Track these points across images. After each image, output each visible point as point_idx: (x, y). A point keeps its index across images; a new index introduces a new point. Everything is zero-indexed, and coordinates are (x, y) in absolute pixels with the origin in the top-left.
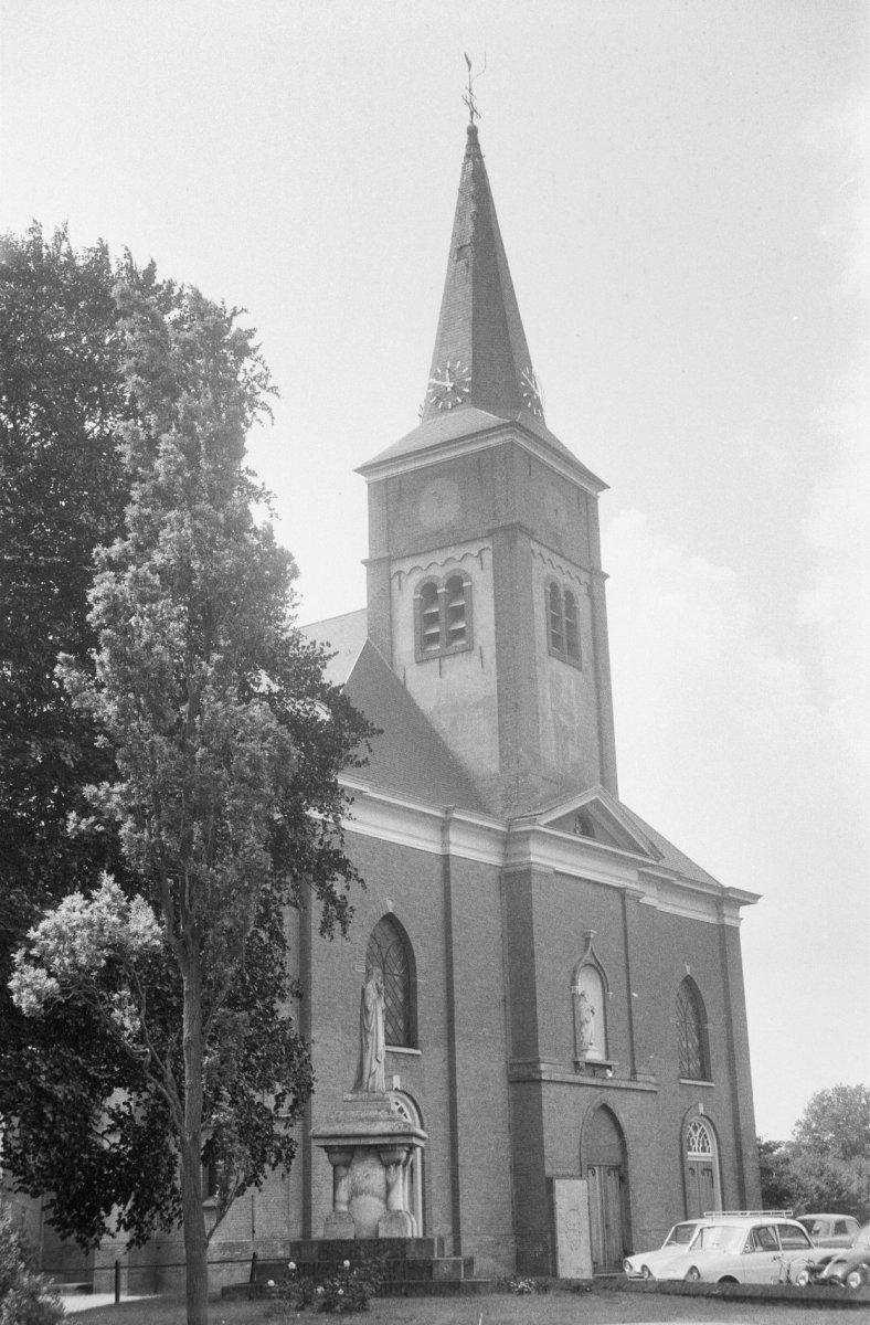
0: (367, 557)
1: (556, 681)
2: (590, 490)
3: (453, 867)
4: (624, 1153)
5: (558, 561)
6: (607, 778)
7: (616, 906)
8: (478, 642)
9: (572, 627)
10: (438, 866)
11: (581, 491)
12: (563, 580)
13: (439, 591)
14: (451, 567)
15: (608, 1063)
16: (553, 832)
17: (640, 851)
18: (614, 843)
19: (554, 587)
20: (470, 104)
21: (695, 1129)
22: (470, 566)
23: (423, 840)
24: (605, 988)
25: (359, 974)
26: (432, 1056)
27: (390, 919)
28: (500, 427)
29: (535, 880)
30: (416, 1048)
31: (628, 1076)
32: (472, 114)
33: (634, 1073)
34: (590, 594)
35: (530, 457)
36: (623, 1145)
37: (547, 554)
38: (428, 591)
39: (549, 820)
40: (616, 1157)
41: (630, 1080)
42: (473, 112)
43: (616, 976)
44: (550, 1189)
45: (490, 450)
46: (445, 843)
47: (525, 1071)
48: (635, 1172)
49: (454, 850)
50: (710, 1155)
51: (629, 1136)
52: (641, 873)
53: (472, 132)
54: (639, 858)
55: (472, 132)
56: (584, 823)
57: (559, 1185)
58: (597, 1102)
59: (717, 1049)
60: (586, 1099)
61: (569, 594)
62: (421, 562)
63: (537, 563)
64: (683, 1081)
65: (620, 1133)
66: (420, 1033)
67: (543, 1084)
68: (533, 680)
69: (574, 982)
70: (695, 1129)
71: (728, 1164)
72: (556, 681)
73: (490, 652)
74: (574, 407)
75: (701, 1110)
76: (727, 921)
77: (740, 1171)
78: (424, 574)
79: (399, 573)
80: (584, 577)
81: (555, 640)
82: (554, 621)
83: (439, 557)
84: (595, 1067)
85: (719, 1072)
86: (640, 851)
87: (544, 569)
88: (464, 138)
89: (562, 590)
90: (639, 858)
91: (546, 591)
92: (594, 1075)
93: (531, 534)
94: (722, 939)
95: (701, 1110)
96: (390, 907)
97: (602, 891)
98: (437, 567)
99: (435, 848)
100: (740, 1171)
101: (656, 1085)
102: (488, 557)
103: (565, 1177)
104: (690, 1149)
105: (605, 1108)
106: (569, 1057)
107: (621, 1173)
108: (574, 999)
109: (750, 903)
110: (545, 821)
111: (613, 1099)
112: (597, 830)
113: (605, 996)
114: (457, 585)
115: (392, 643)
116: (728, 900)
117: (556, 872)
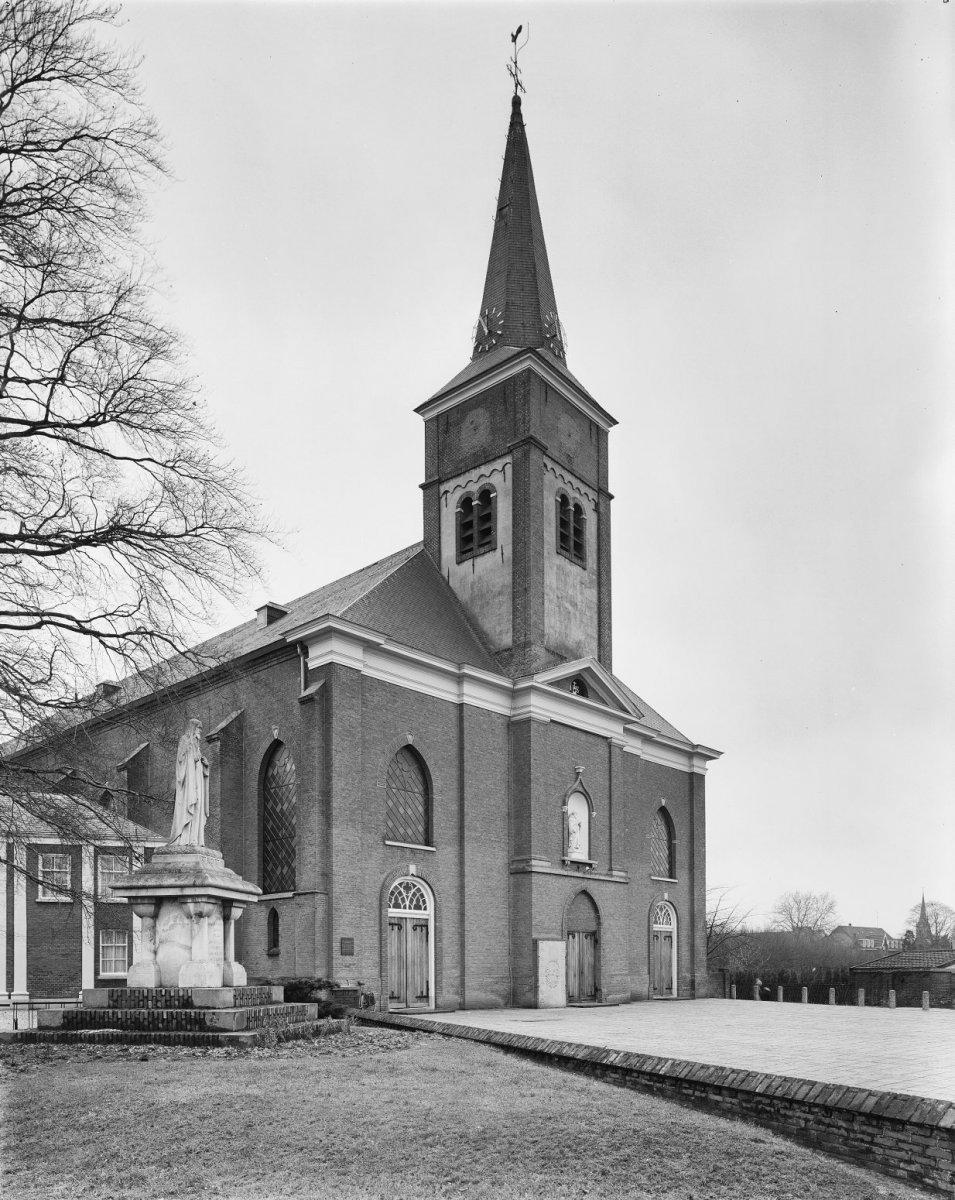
0: (423, 481)
1: (558, 575)
2: (602, 424)
3: (466, 712)
4: (599, 924)
5: (568, 477)
6: (604, 656)
7: (603, 750)
8: (500, 542)
9: (579, 532)
10: (453, 714)
11: (595, 426)
12: (572, 494)
13: (473, 504)
14: (484, 481)
15: (591, 862)
16: (550, 689)
17: (625, 711)
18: (604, 702)
19: (564, 499)
20: (515, 76)
21: (661, 910)
22: (496, 480)
23: (441, 689)
24: (591, 809)
25: (380, 789)
26: (445, 853)
27: (409, 749)
28: (518, 355)
29: (534, 726)
30: (675, 878)
31: (605, 872)
32: (516, 86)
33: (611, 869)
34: (597, 510)
35: (547, 386)
36: (598, 918)
37: (559, 470)
38: (466, 502)
39: (547, 678)
40: (592, 927)
41: (607, 875)
42: (518, 84)
43: (601, 802)
44: (535, 943)
45: (513, 379)
46: (461, 695)
47: (521, 866)
48: (606, 937)
49: (466, 700)
50: (673, 927)
51: (602, 912)
52: (625, 730)
53: (516, 102)
54: (622, 714)
55: (516, 102)
56: (581, 684)
57: (542, 945)
58: (579, 888)
59: (682, 857)
60: (569, 887)
61: (578, 507)
62: (461, 480)
63: (548, 477)
64: (388, 842)
65: (596, 910)
66: (435, 836)
67: (535, 878)
68: (541, 572)
69: (564, 803)
70: (661, 910)
71: (685, 933)
72: (558, 575)
73: (508, 551)
74: (592, 356)
75: (666, 896)
76: (696, 770)
77: (692, 937)
78: (464, 491)
79: (446, 492)
80: (592, 495)
81: (563, 538)
82: (563, 523)
83: (474, 474)
84: (578, 865)
85: (682, 875)
86: (625, 711)
87: (551, 485)
88: (509, 110)
89: (571, 502)
90: (622, 714)
91: (556, 500)
92: (578, 869)
93: (544, 450)
94: (691, 784)
95: (666, 896)
96: (410, 739)
97: (591, 739)
98: (471, 482)
99: (454, 699)
100: (692, 937)
101: (625, 878)
102: (509, 470)
103: (544, 940)
104: (656, 922)
105: (585, 892)
106: (558, 857)
107: (595, 937)
108: (564, 817)
109: (715, 758)
110: (543, 680)
111: (594, 889)
112: (590, 693)
113: (590, 815)
114: (486, 495)
115: (440, 551)
116: (696, 753)
117: (552, 721)
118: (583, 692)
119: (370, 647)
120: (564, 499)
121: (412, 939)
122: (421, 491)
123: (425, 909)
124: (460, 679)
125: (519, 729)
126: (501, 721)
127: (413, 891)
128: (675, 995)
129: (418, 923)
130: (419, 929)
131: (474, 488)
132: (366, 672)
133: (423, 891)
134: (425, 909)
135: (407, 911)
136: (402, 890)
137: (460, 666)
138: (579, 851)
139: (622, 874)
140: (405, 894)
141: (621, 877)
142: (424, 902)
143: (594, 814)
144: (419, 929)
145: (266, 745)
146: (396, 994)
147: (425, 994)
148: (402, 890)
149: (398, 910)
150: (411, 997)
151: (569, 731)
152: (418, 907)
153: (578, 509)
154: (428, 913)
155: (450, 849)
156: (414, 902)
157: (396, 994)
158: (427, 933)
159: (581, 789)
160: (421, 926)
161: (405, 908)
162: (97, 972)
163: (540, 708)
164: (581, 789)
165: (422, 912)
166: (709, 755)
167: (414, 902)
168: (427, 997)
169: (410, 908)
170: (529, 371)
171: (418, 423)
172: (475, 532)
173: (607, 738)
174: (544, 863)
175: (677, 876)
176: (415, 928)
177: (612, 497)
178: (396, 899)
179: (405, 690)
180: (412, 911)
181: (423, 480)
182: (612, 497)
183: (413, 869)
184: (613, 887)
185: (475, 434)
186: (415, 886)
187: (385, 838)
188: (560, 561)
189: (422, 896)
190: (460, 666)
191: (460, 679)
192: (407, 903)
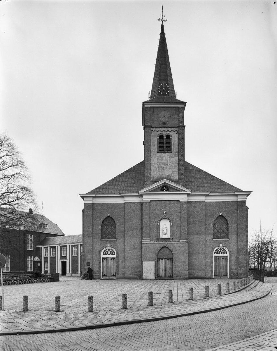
7: (177, 204)
24: (170, 223)
64: (214, 239)
96: (221, 214)
99: (236, 200)
109: (250, 194)
111: (169, 245)
113: (170, 224)
117: (151, 201)
118: (167, 190)
119: (206, 196)
121: (110, 262)
123: (227, 254)
126: (139, 204)
128: (228, 278)
130: (113, 259)
132: (94, 202)
133: (226, 249)
134: (115, 254)
135: (109, 255)
137: (234, 192)
139: (186, 240)
141: (186, 241)
142: (226, 252)
143: (172, 224)
144: (113, 259)
146: (105, 275)
147: (114, 275)
149: (106, 255)
150: (110, 275)
152: (112, 254)
154: (115, 256)
155: (121, 239)
156: (111, 253)
158: (227, 260)
159: (166, 218)
160: (113, 259)
161: (220, 254)
162: (44, 269)
166: (247, 194)
168: (115, 276)
169: (110, 255)
173: (179, 200)
174: (149, 240)
175: (229, 237)
176: (111, 259)
177: (185, 126)
178: (106, 253)
179: (107, 204)
180: (104, 255)
183: (108, 245)
184: (180, 245)
186: (223, 248)
187: (100, 239)
189: (226, 251)
190: (234, 192)
191: (141, 196)
192: (109, 253)
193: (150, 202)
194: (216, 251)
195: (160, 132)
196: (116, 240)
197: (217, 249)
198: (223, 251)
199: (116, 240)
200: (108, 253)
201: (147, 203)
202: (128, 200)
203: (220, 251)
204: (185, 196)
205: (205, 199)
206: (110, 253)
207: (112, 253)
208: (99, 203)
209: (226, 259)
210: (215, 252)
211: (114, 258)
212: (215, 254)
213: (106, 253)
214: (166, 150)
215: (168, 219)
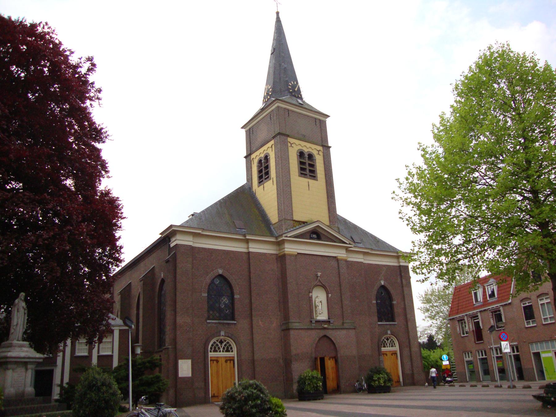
7: (334, 263)
14: (265, 152)
21: (388, 339)
24: (327, 294)
38: (260, 162)
60: (315, 335)
64: (208, 321)
74: (312, 94)
83: (261, 150)
96: (221, 272)
99: (245, 250)
111: (329, 333)
114: (266, 158)
117: (298, 253)
118: (319, 238)
119: (365, 253)
120: (301, 154)
122: (245, 159)
123: (232, 351)
124: (247, 241)
125: (282, 258)
127: (224, 343)
129: (228, 358)
130: (229, 362)
131: (262, 156)
132: (349, 259)
133: (230, 343)
134: (232, 351)
135: (221, 353)
136: (218, 343)
138: (322, 315)
140: (220, 345)
142: (231, 348)
144: (229, 362)
145: (159, 281)
148: (218, 343)
149: (216, 353)
151: (313, 257)
152: (227, 351)
153: (311, 156)
157: (216, 395)
159: (320, 284)
160: (230, 360)
161: (220, 351)
163: (290, 249)
164: (320, 284)
165: (231, 353)
167: (213, 349)
169: (223, 351)
170: (278, 107)
171: (244, 131)
172: (264, 173)
176: (392, 355)
177: (330, 147)
178: (215, 348)
181: (245, 155)
182: (330, 147)
185: (263, 134)
188: (304, 181)
189: (230, 345)
190: (245, 236)
191: (247, 241)
192: (222, 350)
193: (296, 255)
194: (212, 345)
195: (300, 147)
196: (235, 322)
197: (214, 343)
198: (225, 345)
199: (235, 322)
200: (219, 348)
201: (291, 255)
202: (255, 248)
203: (220, 345)
204: (344, 251)
205: (194, 243)
206: (224, 348)
207: (228, 348)
208: (203, 248)
209: (232, 362)
210: (211, 348)
211: (232, 360)
212: (211, 352)
213: (215, 348)
214: (310, 176)
215: (324, 287)
